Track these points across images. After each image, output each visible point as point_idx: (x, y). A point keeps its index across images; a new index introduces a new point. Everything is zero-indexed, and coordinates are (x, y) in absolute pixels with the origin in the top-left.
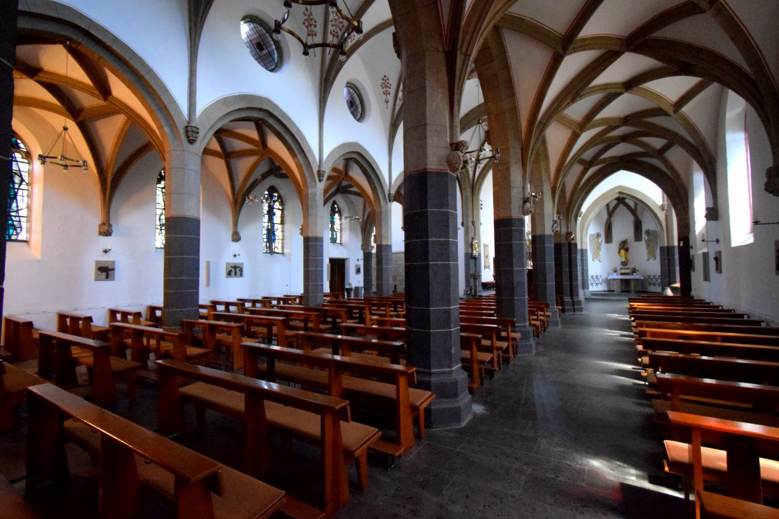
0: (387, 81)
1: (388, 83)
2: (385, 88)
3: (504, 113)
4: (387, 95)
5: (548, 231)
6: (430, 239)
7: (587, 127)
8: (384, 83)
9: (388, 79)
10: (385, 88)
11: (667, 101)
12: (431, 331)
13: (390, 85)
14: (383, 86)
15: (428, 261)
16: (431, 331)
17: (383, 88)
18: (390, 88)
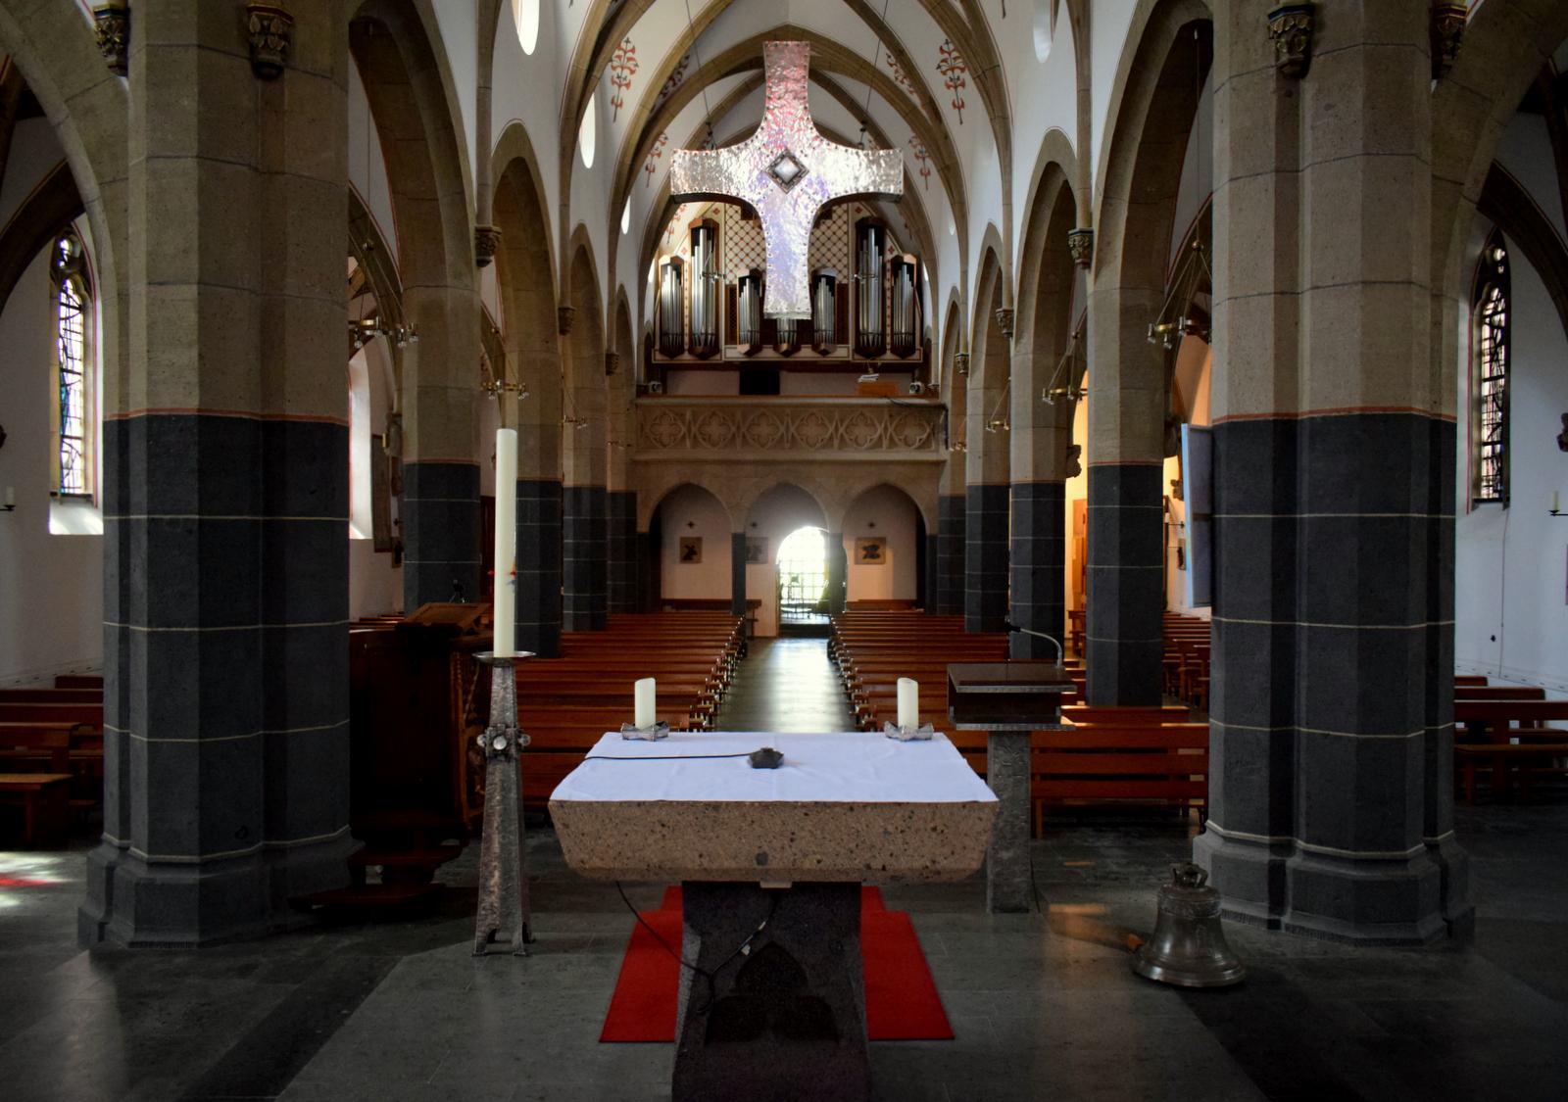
0: (629, 55)
1: (630, 59)
2: (950, 73)
3: (1315, 288)
4: (956, 87)
5: (570, 472)
6: (1268, 729)
7: (1204, 307)
8: (944, 61)
9: (633, 50)
10: (950, 73)
11: (712, 609)
12: (1442, 623)
13: (636, 65)
14: (944, 69)
15: (1272, 732)
16: (1442, 623)
17: (944, 73)
18: (632, 72)
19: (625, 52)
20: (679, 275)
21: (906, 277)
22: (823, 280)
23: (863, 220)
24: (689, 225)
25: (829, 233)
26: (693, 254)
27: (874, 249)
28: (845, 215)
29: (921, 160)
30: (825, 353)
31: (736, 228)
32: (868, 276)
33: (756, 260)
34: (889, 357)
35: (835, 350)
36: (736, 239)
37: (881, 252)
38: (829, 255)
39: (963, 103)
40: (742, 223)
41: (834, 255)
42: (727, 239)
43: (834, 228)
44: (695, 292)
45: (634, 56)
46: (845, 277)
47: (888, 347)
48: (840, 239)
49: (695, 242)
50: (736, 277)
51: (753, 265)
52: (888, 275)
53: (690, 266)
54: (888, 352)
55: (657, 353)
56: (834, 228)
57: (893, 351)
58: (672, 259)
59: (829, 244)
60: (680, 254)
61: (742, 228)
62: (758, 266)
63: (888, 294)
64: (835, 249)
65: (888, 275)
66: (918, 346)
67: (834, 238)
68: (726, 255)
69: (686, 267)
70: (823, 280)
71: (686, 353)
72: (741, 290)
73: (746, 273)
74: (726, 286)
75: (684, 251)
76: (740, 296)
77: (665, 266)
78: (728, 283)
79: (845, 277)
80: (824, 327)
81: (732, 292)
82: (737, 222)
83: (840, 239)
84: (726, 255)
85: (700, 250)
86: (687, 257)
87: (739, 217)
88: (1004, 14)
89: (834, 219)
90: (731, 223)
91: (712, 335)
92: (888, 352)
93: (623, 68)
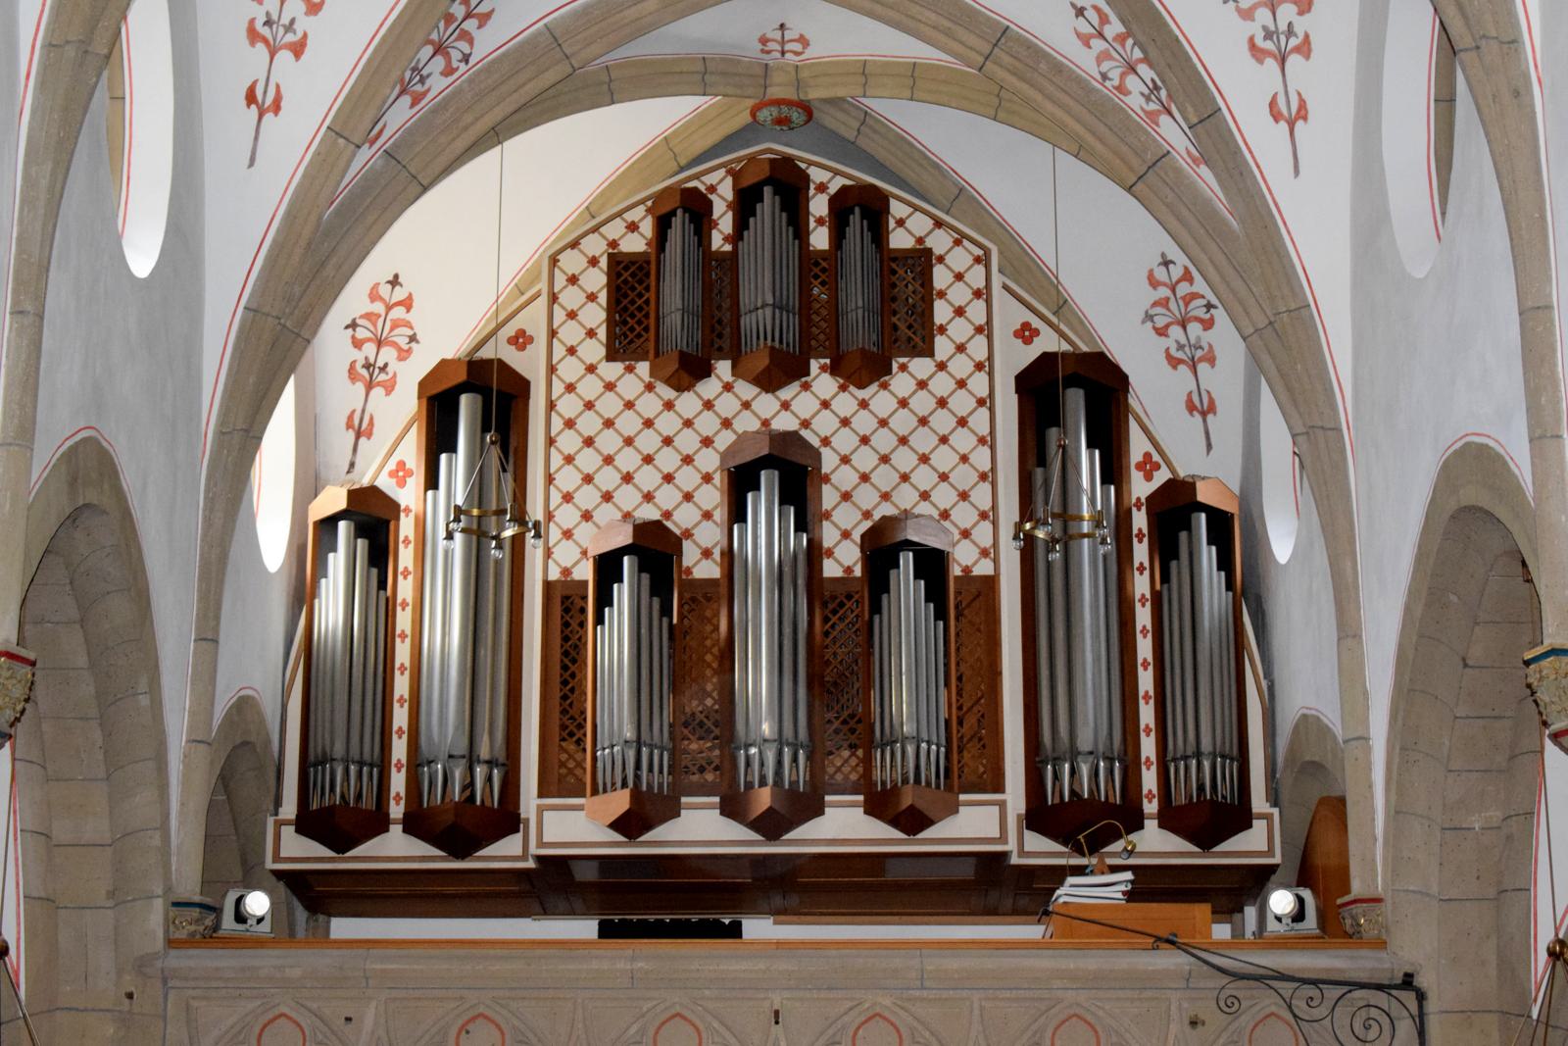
0: (398, 313)
9: (407, 304)
13: (413, 339)
14: (1160, 322)
19: (389, 308)
20: (380, 554)
21: (1208, 555)
22: (907, 560)
23: (1047, 359)
24: (422, 385)
25: (923, 403)
26: (432, 482)
27: (1087, 463)
28: (980, 269)
29: (1271, 64)
30: (913, 821)
31: (590, 387)
32: (1067, 539)
33: (659, 497)
34: (1155, 842)
35: (953, 809)
36: (589, 424)
37: (1113, 472)
38: (924, 478)
39: (1212, 402)
40: (613, 370)
41: (944, 477)
42: (557, 424)
43: (942, 384)
44: (433, 638)
45: (409, 317)
46: (984, 553)
47: (1151, 807)
48: (962, 422)
49: (439, 438)
50: (584, 553)
51: (650, 513)
52: (1141, 552)
53: (421, 524)
54: (1151, 825)
55: (288, 832)
56: (942, 384)
57: (1170, 819)
58: (354, 495)
59: (923, 441)
60: (385, 483)
61: (610, 387)
62: (668, 515)
63: (1143, 617)
64: (944, 459)
65: (1141, 552)
66: (1259, 802)
67: (943, 421)
68: (550, 479)
69: (406, 527)
70: (907, 560)
71: (396, 830)
72: (604, 599)
73: (623, 537)
74: (548, 586)
75: (401, 473)
76: (599, 620)
77: (329, 524)
78: (554, 575)
79: (984, 553)
80: (908, 729)
81: (564, 601)
82: (591, 369)
83: (962, 422)
84: (550, 479)
85: (456, 468)
86: (408, 495)
87: (602, 352)
88: (1209, 446)
89: (940, 355)
90: (570, 370)
91: (491, 763)
92: (1151, 825)
93: (380, 343)
